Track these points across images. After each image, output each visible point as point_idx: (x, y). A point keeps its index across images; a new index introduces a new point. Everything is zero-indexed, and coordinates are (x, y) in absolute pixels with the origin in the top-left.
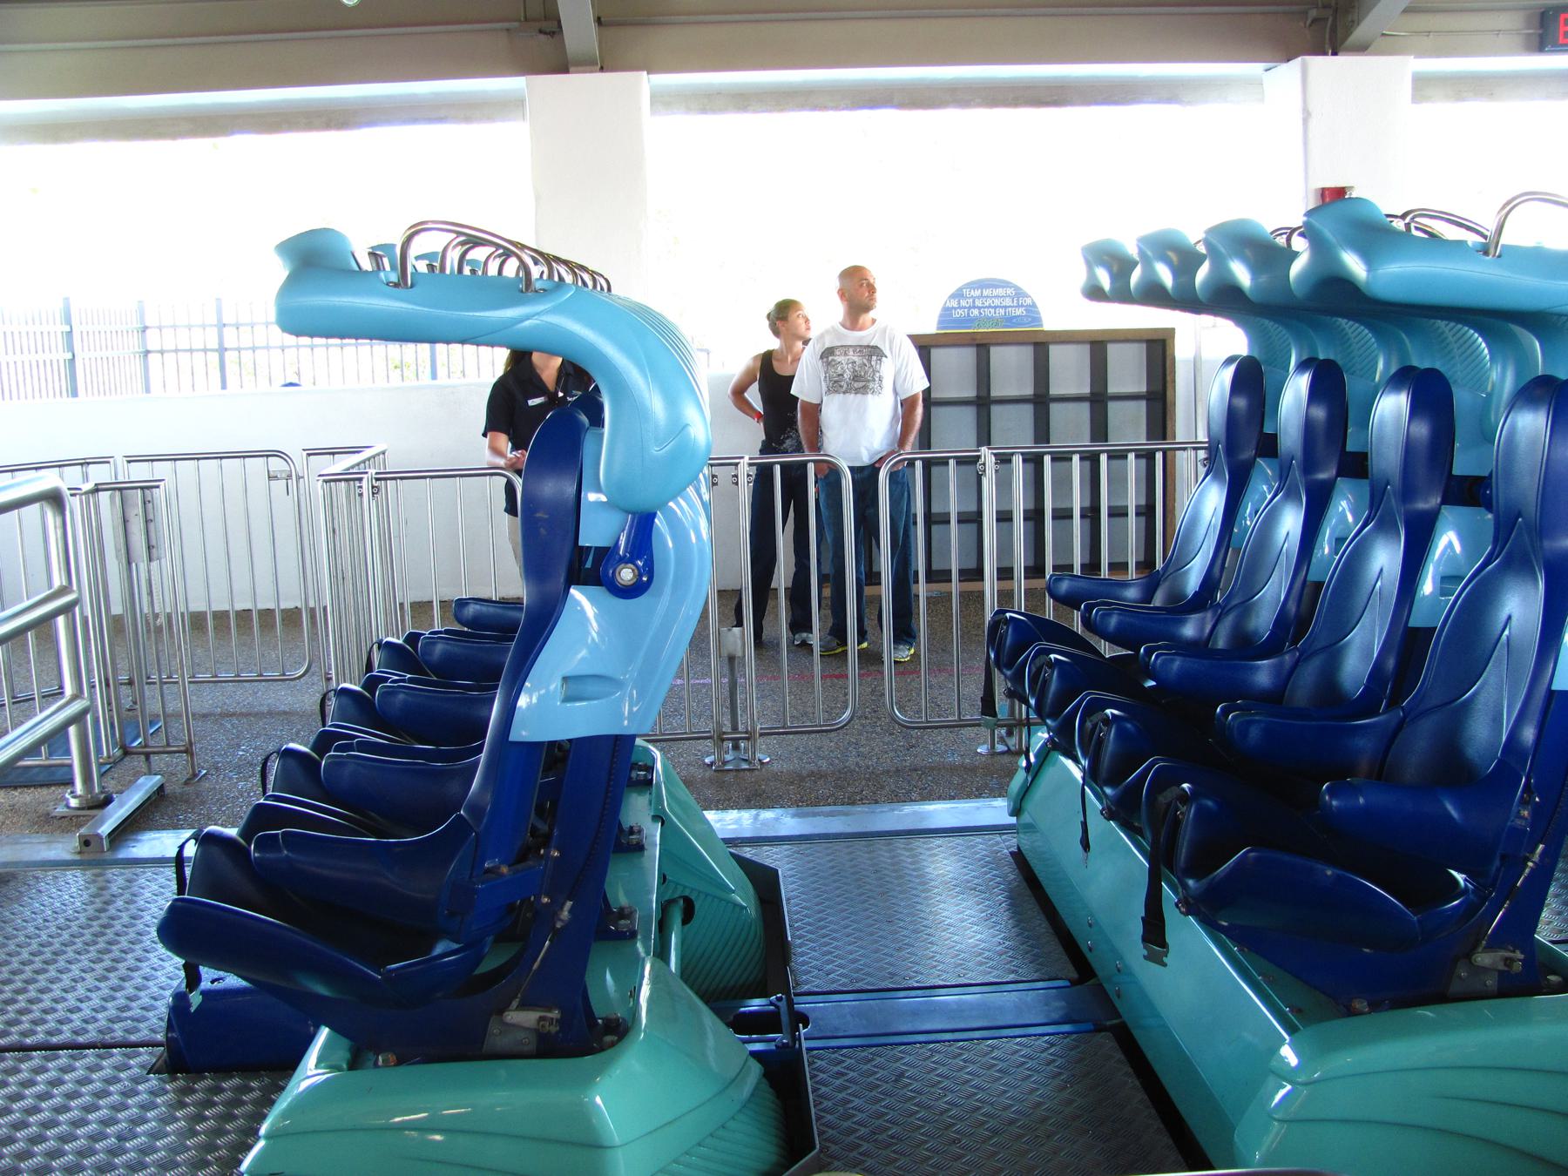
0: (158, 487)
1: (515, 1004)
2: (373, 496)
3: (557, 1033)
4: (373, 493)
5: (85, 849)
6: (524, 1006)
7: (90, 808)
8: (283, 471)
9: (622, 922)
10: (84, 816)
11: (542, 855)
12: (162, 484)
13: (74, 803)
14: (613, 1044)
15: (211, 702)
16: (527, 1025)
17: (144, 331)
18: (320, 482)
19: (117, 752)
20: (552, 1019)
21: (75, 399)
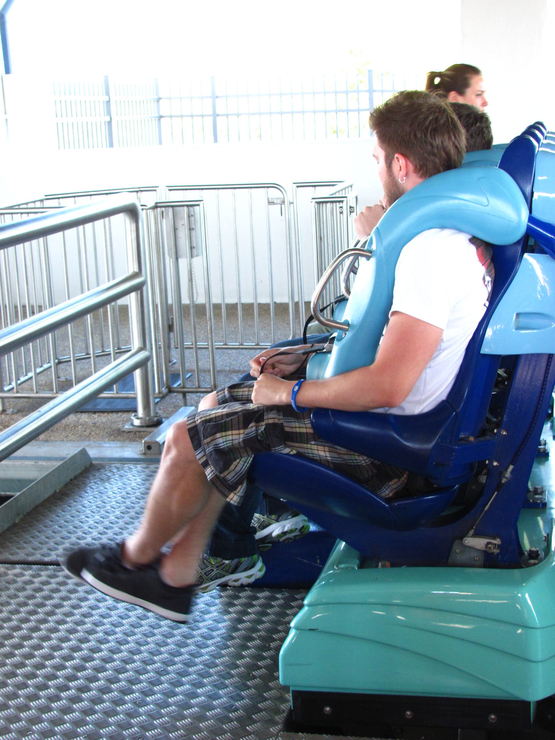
0: (198, 205)
1: (471, 532)
2: (350, 214)
3: (498, 554)
4: (351, 212)
5: (148, 452)
6: (476, 535)
7: (148, 426)
8: (279, 198)
9: (537, 496)
10: (144, 432)
11: (495, 434)
12: (201, 203)
13: (137, 422)
14: (535, 564)
15: (221, 363)
16: (478, 547)
17: (158, 101)
18: (314, 203)
19: (164, 390)
20: (495, 544)
21: (111, 148)
